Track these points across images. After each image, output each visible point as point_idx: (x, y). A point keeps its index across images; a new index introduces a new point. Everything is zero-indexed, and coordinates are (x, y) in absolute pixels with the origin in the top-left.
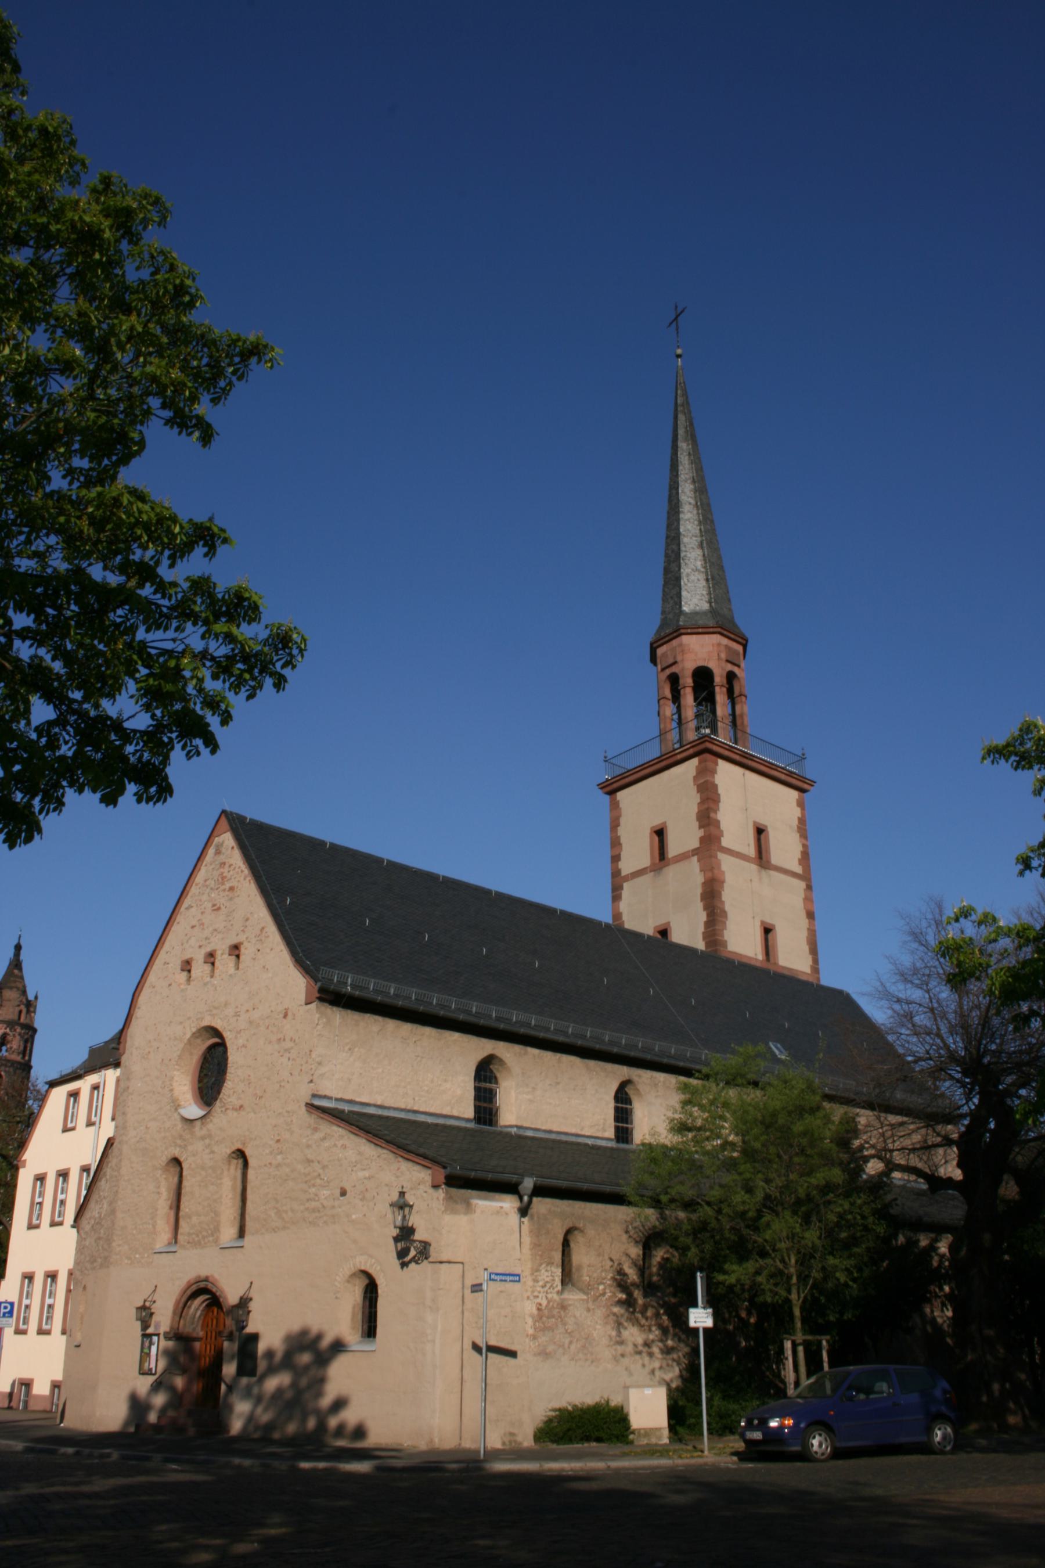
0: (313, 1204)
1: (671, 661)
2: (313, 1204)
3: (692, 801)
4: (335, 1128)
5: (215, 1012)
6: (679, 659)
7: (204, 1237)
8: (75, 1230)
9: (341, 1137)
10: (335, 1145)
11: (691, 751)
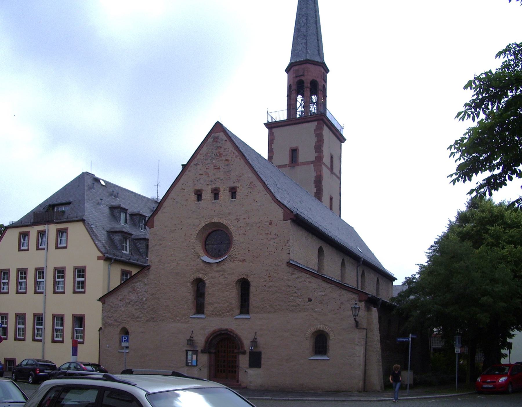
0: (293, 304)
1: (301, 74)
2: (293, 304)
3: (313, 140)
4: (304, 274)
5: (221, 216)
6: (306, 73)
7: (223, 313)
8: (100, 303)
9: (309, 278)
10: (304, 281)
11: (315, 118)
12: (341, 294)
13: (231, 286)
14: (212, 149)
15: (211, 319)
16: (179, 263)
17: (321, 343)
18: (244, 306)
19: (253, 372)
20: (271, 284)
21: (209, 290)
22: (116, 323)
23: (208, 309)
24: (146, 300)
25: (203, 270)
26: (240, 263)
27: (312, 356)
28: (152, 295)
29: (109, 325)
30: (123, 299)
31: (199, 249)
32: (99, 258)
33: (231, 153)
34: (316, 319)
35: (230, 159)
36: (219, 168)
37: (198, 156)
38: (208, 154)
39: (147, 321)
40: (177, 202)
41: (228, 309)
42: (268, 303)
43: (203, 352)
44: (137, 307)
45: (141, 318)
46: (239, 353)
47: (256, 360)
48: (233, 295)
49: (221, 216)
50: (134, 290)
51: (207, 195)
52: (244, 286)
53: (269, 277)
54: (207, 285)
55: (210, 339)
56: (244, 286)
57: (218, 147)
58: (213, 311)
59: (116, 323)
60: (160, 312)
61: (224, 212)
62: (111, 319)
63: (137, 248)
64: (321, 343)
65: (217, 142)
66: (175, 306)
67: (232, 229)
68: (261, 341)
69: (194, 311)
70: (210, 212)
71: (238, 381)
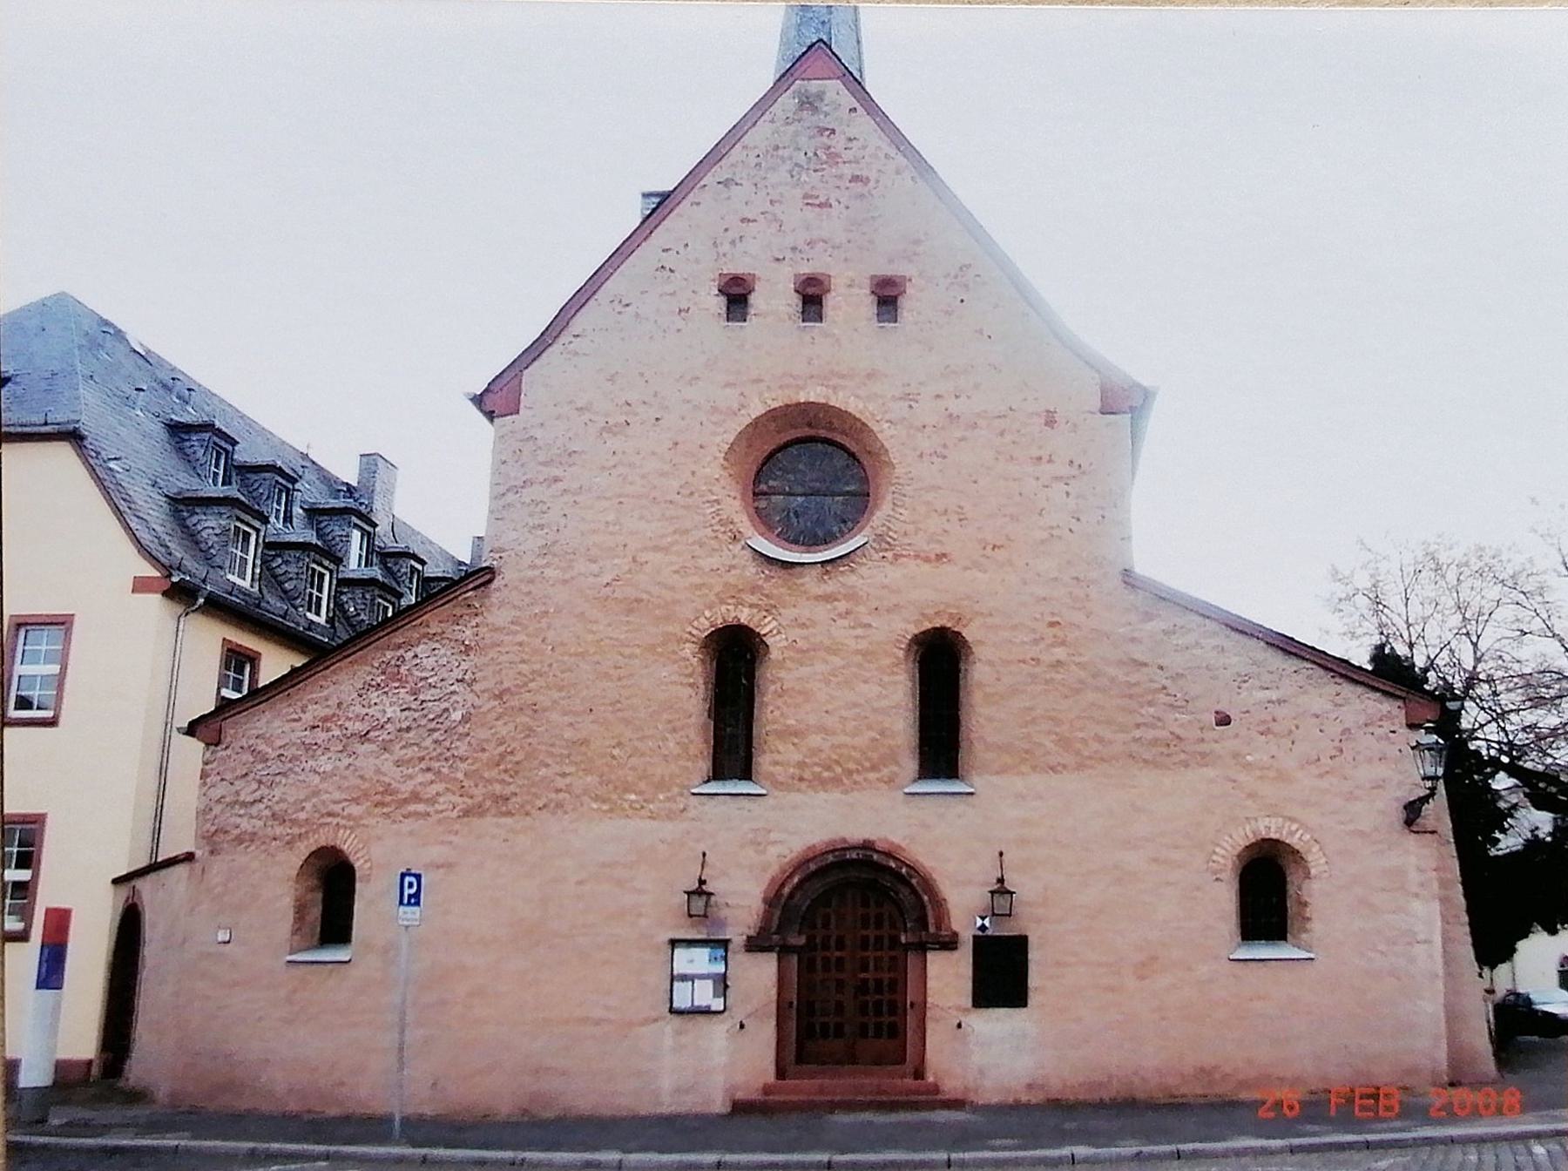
2: (1151, 734)
5: (834, 381)
7: (850, 773)
9: (1215, 633)
12: (1338, 700)
13: (888, 661)
14: (796, 134)
15: (795, 797)
16: (642, 557)
17: (1266, 893)
18: (940, 746)
19: (996, 1023)
20: (1060, 653)
21: (782, 674)
22: (279, 830)
23: (774, 755)
24: (466, 719)
25: (754, 589)
26: (926, 567)
27: (307, 949)
28: (499, 696)
29: (239, 840)
30: (326, 719)
31: (735, 509)
32: (141, 585)
33: (876, 156)
34: (1251, 796)
35: (873, 175)
36: (826, 205)
37: (737, 153)
38: (777, 148)
39: (467, 813)
40: (637, 315)
41: (875, 756)
42: (1049, 733)
43: (754, 945)
44: (410, 753)
45: (432, 801)
46: (922, 948)
47: (1002, 974)
48: (894, 699)
49: (834, 381)
50: (396, 677)
51: (774, 299)
52: (939, 661)
53: (1052, 624)
54: (774, 654)
55: (786, 890)
56: (939, 661)
57: (821, 131)
58: (801, 765)
59: (279, 830)
60: (543, 772)
61: (842, 365)
62: (254, 810)
63: (275, 577)
64: (1266, 893)
65: (815, 110)
66: (619, 744)
67: (886, 434)
68: (1023, 885)
69: (705, 766)
70: (780, 363)
71: (919, 1074)
